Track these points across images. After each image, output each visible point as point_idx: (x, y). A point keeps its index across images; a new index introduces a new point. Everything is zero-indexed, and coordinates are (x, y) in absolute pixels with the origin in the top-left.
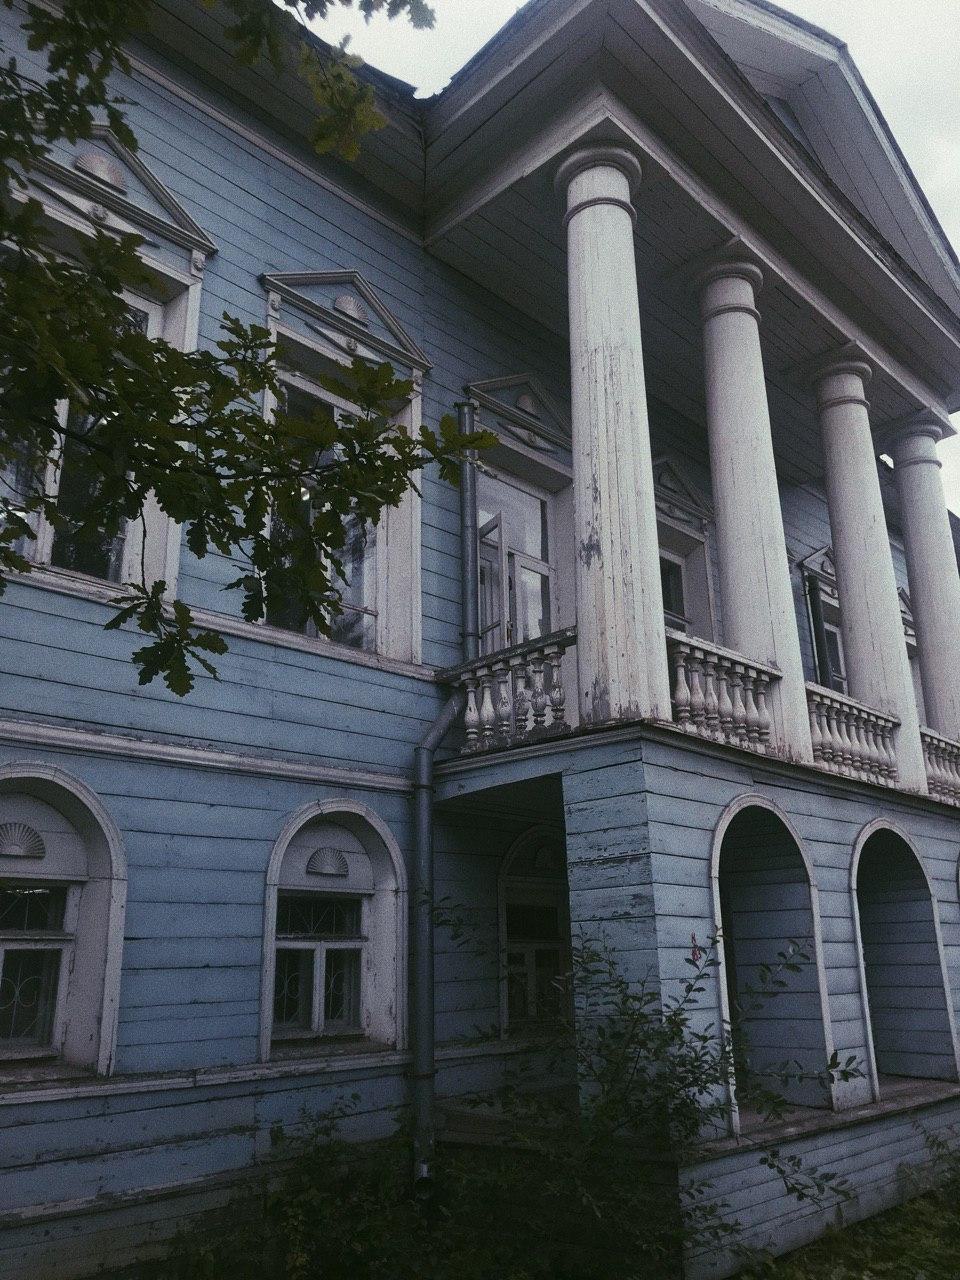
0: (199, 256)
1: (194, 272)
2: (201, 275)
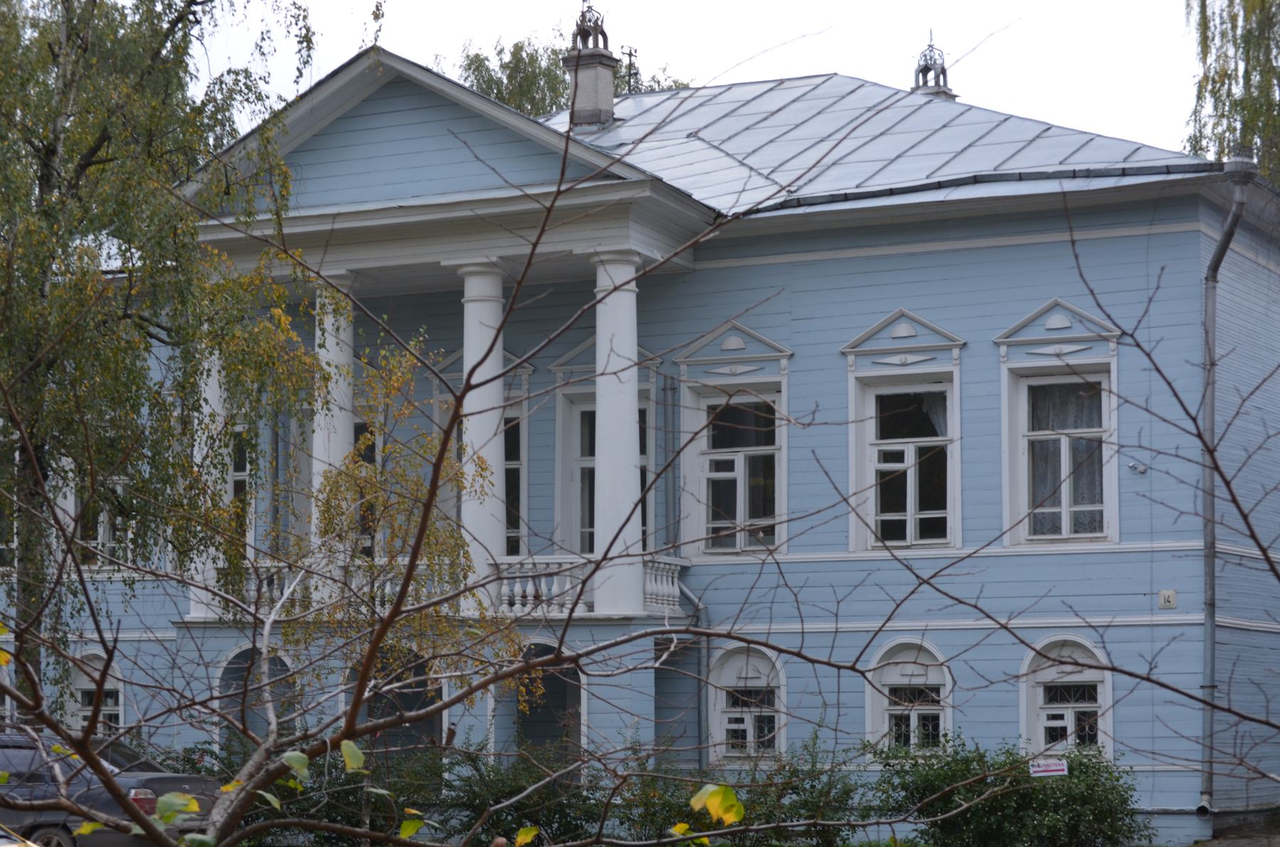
0: (956, 352)
1: (1111, 353)
2: (1115, 353)
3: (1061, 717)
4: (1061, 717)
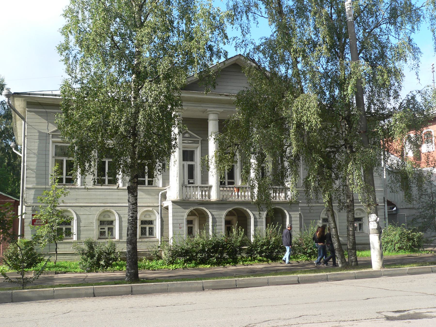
3: (104, 229)
4: (104, 229)
